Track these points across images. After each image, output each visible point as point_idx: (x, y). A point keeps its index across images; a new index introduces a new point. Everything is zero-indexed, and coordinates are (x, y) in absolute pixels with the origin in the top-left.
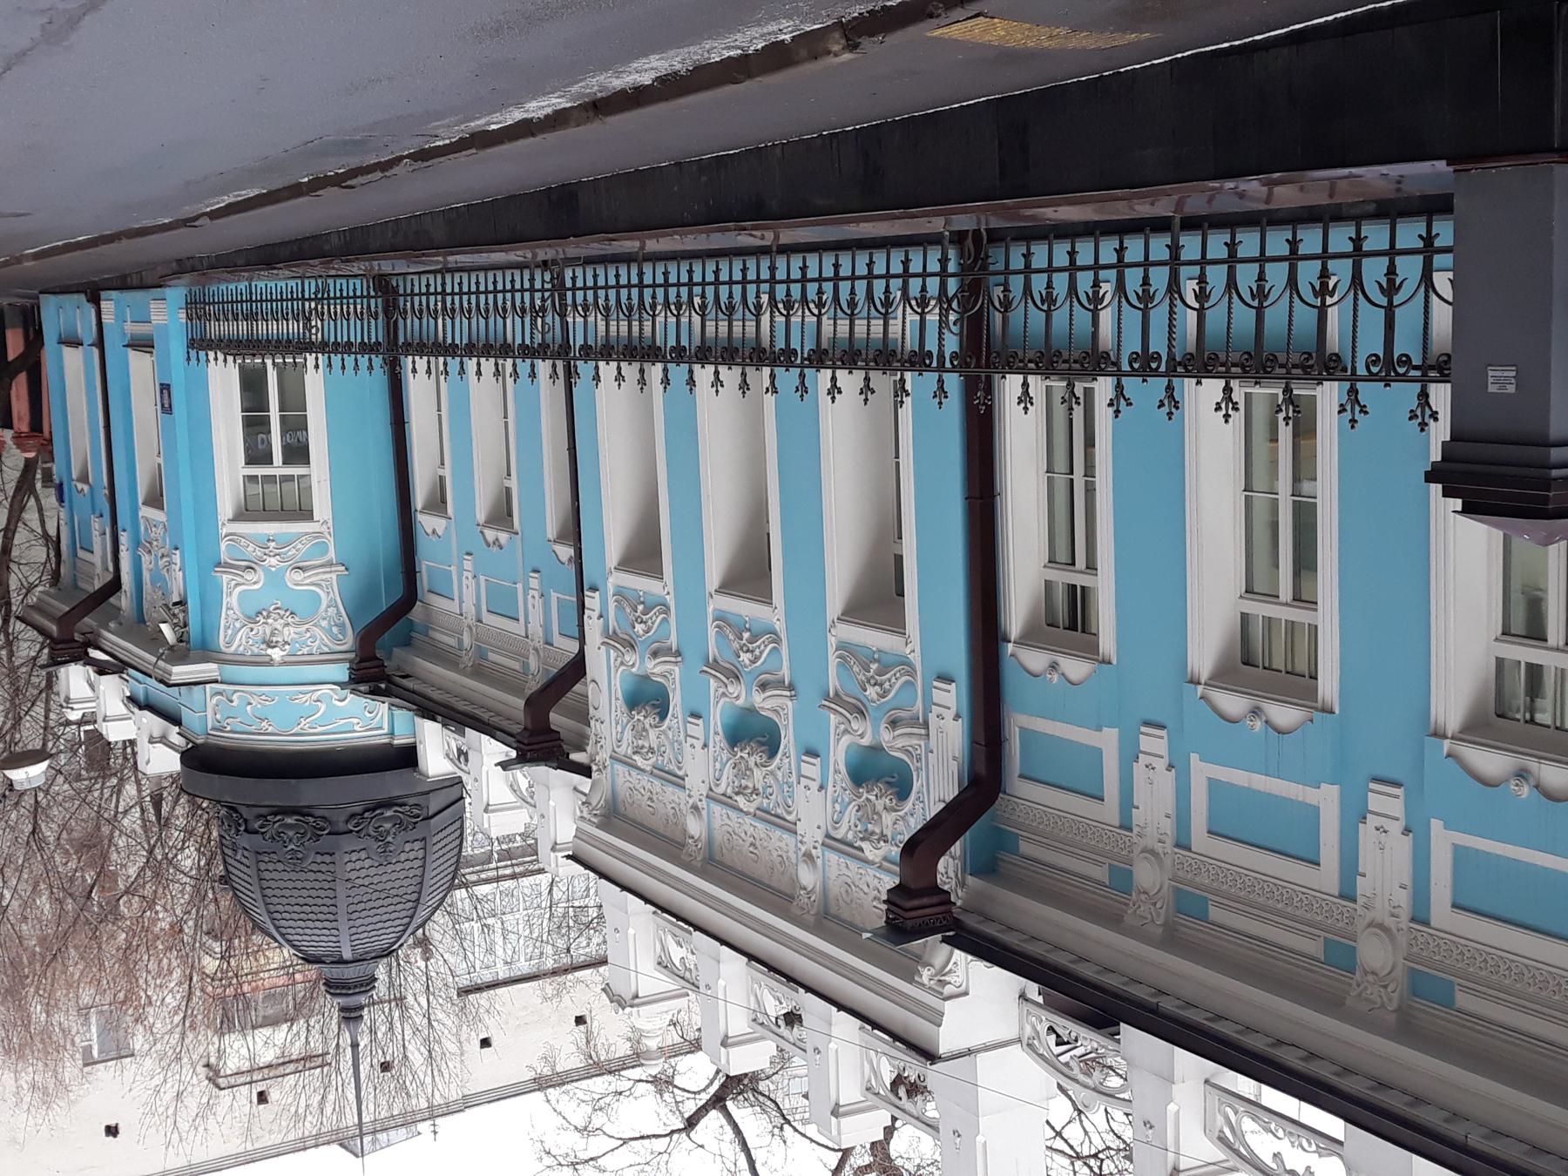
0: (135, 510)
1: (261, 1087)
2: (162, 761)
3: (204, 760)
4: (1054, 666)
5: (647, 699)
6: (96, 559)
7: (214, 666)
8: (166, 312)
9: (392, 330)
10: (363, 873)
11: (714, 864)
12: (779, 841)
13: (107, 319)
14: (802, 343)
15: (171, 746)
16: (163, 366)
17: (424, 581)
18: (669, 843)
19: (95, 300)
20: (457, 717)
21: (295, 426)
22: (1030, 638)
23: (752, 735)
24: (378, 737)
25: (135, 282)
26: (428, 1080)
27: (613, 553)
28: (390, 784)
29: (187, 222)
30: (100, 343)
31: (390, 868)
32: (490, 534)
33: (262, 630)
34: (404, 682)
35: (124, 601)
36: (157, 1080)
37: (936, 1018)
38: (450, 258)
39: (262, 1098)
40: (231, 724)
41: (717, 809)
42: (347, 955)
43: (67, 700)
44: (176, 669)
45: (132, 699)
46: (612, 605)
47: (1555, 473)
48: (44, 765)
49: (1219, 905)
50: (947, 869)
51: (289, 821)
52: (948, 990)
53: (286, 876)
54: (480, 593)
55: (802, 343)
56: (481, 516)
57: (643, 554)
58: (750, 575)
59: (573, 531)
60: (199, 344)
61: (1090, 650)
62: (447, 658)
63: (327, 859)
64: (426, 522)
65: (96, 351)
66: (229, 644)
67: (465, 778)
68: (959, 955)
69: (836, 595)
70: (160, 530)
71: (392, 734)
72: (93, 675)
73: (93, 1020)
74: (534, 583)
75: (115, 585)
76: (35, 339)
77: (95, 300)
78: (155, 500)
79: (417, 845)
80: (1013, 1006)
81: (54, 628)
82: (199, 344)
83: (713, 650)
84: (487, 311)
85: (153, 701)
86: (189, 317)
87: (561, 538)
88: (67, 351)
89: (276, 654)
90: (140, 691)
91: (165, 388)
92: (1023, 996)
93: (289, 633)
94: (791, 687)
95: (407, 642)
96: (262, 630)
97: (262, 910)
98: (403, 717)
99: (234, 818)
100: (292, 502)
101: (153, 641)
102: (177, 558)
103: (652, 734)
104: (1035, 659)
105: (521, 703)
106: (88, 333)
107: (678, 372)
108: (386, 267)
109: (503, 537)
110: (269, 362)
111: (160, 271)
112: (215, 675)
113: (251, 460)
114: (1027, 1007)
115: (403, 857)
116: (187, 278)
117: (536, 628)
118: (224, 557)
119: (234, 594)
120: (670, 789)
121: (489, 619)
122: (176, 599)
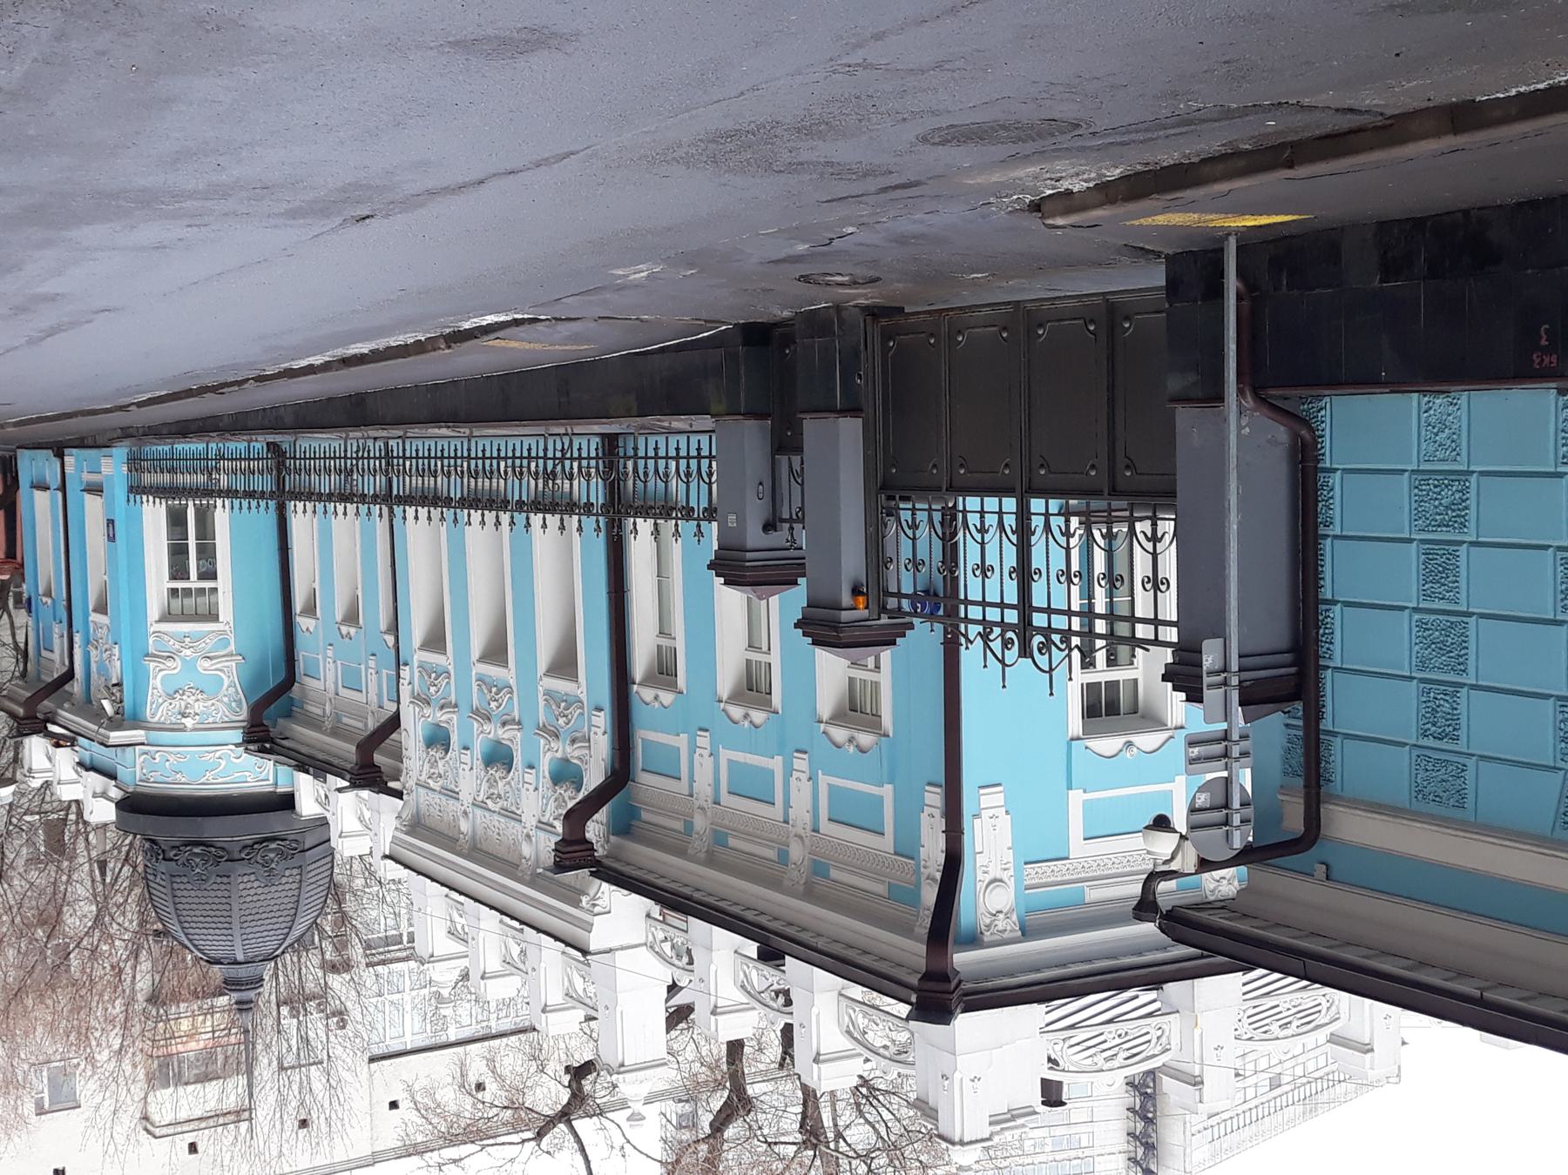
0: (86, 616)
1: (190, 1138)
2: (103, 812)
3: (134, 805)
4: (656, 698)
5: (438, 740)
6: (56, 656)
7: (142, 732)
8: (113, 466)
9: (280, 482)
10: (252, 892)
11: (477, 852)
12: (514, 829)
13: (68, 470)
14: (456, 494)
15: (110, 799)
16: (109, 506)
17: (300, 667)
18: (447, 839)
19: (60, 455)
20: (316, 766)
21: (207, 552)
22: (648, 681)
23: (499, 758)
24: (265, 787)
25: (90, 441)
26: (327, 1105)
27: (417, 640)
28: (274, 823)
29: (122, 408)
30: (63, 488)
31: (273, 889)
32: (344, 629)
33: (178, 704)
34: (285, 743)
35: (76, 687)
36: (98, 1099)
37: (589, 928)
38: (179, 447)
39: (193, 1148)
40: (154, 776)
41: (478, 812)
42: (240, 957)
43: (30, 770)
44: (113, 734)
45: (80, 764)
46: (417, 674)
47: (749, 555)
48: (12, 788)
49: (735, 837)
50: (594, 830)
51: (197, 850)
52: (597, 909)
53: (193, 893)
54: (336, 677)
55: (456, 494)
56: (339, 618)
57: (435, 641)
58: (496, 652)
59: (394, 628)
60: (136, 489)
61: (672, 686)
62: (314, 723)
63: (225, 880)
64: (303, 622)
65: (60, 494)
66: (153, 715)
67: (328, 815)
68: (605, 886)
69: (543, 663)
70: (105, 630)
71: (276, 784)
72: (50, 748)
73: (45, 1073)
74: (372, 664)
75: (69, 675)
76: (13, 484)
77: (60, 455)
78: (102, 608)
79: (295, 872)
80: (642, 922)
81: (21, 711)
82: (136, 489)
83: (475, 703)
84: (646, 474)
85: (95, 763)
86: (130, 471)
87: (388, 632)
88: (38, 494)
89: (189, 722)
90: (86, 756)
91: (111, 523)
92: (648, 916)
93: (198, 707)
94: (519, 723)
95: (289, 714)
96: (178, 704)
97: (175, 921)
98: (283, 770)
99: (155, 849)
100: (202, 610)
101: (97, 715)
102: (116, 651)
103: (440, 763)
104: (647, 694)
105: (353, 749)
106: (55, 482)
107: (520, 518)
108: (277, 438)
109: (353, 631)
110: (191, 503)
111: (109, 435)
112: (143, 739)
113: (173, 577)
114: (651, 921)
115: (284, 880)
116: (127, 442)
117: (373, 697)
118: (151, 650)
119: (158, 677)
120: (452, 802)
121: (343, 692)
122: (114, 681)
